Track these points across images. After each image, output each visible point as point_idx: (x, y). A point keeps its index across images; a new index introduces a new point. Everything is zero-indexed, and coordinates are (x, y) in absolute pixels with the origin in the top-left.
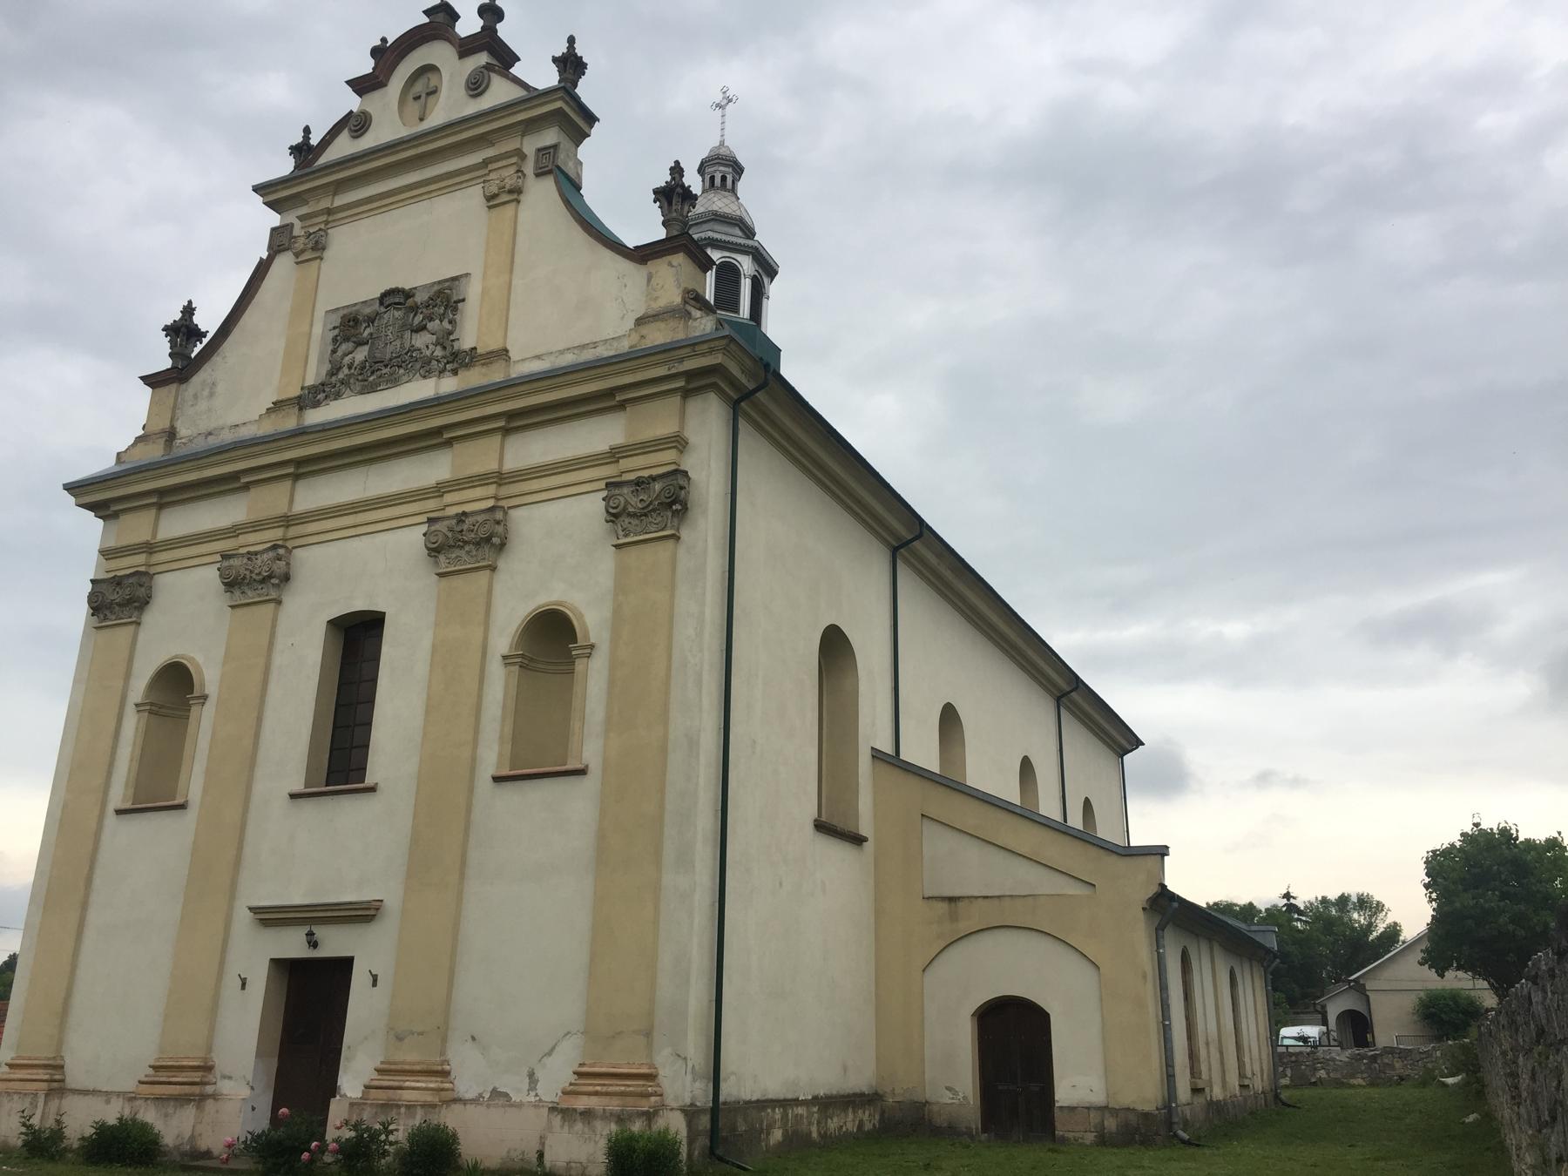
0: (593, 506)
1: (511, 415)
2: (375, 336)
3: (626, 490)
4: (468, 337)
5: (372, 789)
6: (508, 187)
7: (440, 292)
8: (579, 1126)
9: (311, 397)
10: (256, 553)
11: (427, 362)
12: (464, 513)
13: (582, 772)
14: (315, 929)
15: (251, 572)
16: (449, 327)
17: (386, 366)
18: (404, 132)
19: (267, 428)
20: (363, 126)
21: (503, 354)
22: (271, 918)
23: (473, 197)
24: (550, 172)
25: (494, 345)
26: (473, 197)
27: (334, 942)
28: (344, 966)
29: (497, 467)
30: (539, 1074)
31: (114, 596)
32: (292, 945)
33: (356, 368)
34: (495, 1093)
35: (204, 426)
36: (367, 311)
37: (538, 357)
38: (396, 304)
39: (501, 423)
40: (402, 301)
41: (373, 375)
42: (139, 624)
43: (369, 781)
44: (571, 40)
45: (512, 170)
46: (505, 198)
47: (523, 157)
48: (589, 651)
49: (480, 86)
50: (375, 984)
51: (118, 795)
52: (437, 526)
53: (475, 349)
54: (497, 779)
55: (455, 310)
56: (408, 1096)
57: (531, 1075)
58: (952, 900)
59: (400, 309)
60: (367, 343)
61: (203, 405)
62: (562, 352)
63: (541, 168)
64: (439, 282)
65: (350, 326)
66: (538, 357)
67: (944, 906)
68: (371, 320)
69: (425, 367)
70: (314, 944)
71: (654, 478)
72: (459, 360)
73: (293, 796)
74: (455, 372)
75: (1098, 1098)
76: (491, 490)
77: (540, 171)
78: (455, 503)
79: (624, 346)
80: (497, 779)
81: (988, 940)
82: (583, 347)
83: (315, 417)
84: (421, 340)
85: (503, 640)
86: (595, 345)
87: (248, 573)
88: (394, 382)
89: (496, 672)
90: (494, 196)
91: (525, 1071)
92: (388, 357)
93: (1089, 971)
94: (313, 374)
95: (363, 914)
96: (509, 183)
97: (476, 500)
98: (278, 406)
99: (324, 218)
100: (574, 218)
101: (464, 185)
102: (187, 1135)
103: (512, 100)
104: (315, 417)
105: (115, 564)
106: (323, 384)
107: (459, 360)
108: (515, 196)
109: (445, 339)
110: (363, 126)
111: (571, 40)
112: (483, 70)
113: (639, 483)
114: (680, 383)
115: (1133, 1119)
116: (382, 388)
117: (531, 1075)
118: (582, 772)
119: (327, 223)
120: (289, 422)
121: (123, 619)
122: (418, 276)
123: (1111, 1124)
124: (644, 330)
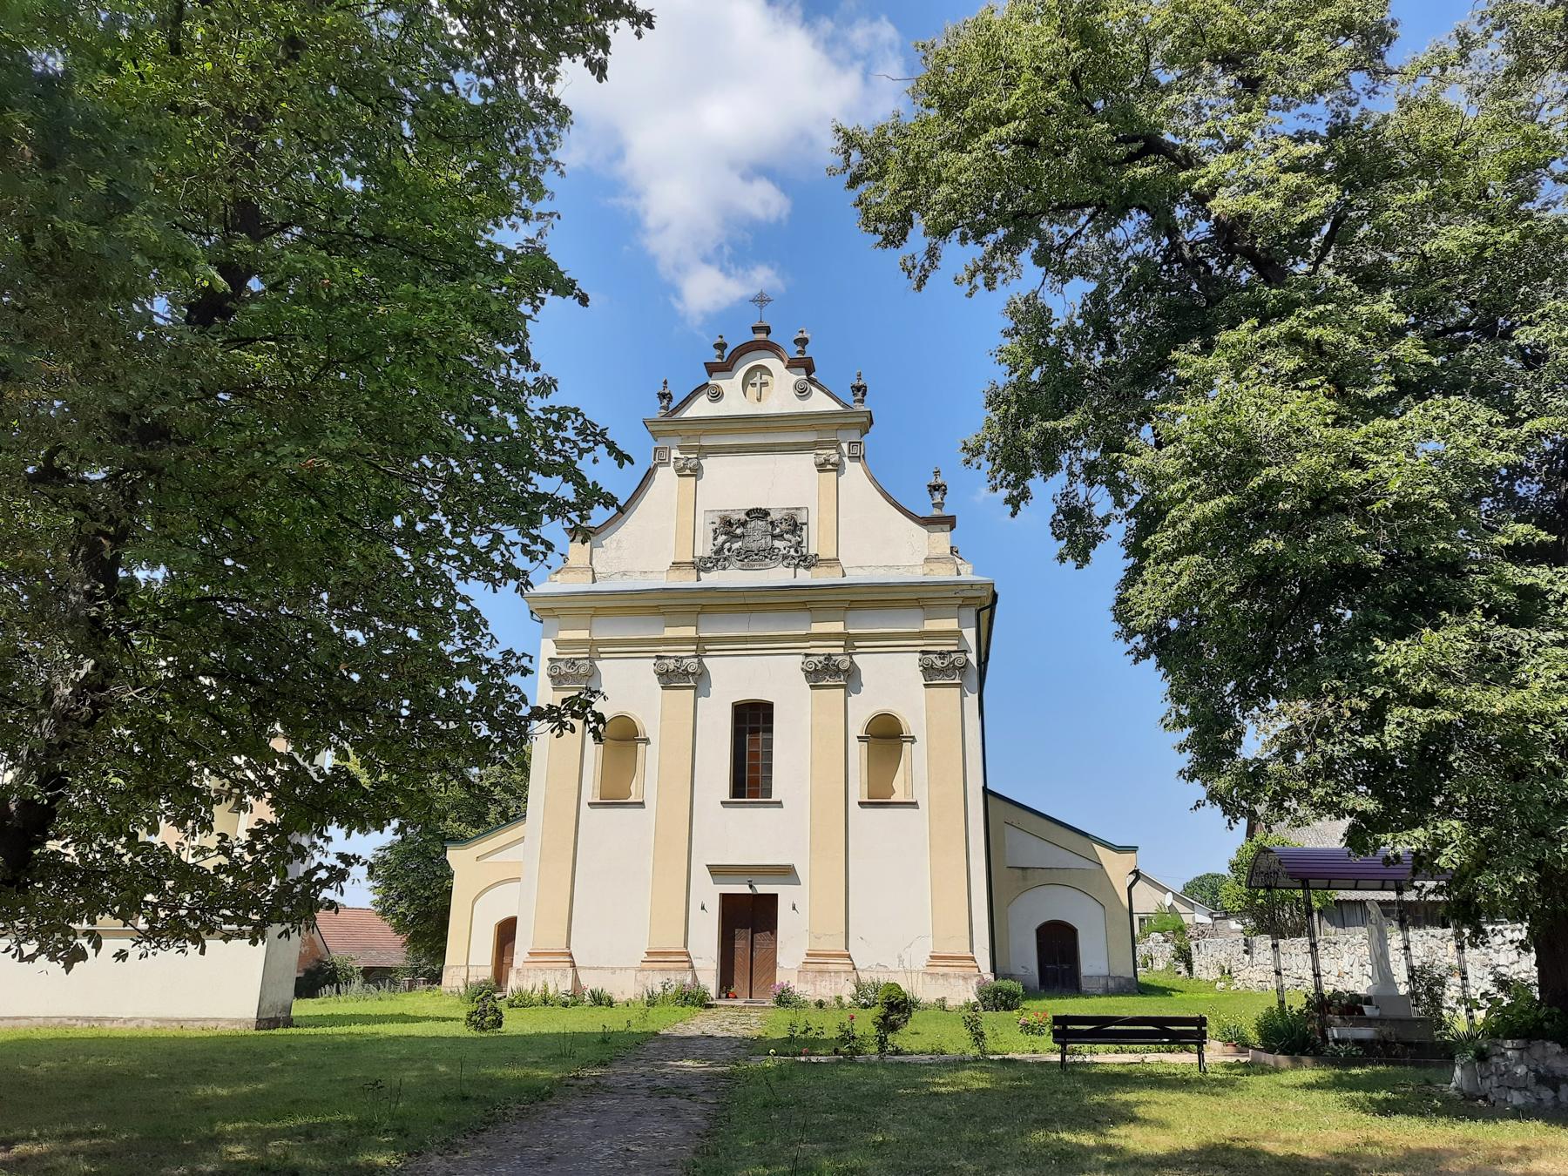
5: (779, 804)
8: (941, 981)
9: (701, 566)
13: (641, 805)
22: (717, 872)
26: (807, 461)
28: (773, 898)
36: (737, 517)
41: (749, 558)
43: (774, 798)
46: (829, 467)
51: (590, 793)
52: (810, 659)
54: (861, 804)
65: (728, 526)
67: (1020, 871)
68: (743, 524)
72: (808, 561)
75: (1105, 972)
85: (858, 728)
94: (705, 549)
95: (786, 873)
98: (677, 565)
107: (808, 561)
115: (1123, 981)
118: (914, 805)
120: (687, 580)
122: (777, 502)
123: (1111, 984)
124: (934, 566)
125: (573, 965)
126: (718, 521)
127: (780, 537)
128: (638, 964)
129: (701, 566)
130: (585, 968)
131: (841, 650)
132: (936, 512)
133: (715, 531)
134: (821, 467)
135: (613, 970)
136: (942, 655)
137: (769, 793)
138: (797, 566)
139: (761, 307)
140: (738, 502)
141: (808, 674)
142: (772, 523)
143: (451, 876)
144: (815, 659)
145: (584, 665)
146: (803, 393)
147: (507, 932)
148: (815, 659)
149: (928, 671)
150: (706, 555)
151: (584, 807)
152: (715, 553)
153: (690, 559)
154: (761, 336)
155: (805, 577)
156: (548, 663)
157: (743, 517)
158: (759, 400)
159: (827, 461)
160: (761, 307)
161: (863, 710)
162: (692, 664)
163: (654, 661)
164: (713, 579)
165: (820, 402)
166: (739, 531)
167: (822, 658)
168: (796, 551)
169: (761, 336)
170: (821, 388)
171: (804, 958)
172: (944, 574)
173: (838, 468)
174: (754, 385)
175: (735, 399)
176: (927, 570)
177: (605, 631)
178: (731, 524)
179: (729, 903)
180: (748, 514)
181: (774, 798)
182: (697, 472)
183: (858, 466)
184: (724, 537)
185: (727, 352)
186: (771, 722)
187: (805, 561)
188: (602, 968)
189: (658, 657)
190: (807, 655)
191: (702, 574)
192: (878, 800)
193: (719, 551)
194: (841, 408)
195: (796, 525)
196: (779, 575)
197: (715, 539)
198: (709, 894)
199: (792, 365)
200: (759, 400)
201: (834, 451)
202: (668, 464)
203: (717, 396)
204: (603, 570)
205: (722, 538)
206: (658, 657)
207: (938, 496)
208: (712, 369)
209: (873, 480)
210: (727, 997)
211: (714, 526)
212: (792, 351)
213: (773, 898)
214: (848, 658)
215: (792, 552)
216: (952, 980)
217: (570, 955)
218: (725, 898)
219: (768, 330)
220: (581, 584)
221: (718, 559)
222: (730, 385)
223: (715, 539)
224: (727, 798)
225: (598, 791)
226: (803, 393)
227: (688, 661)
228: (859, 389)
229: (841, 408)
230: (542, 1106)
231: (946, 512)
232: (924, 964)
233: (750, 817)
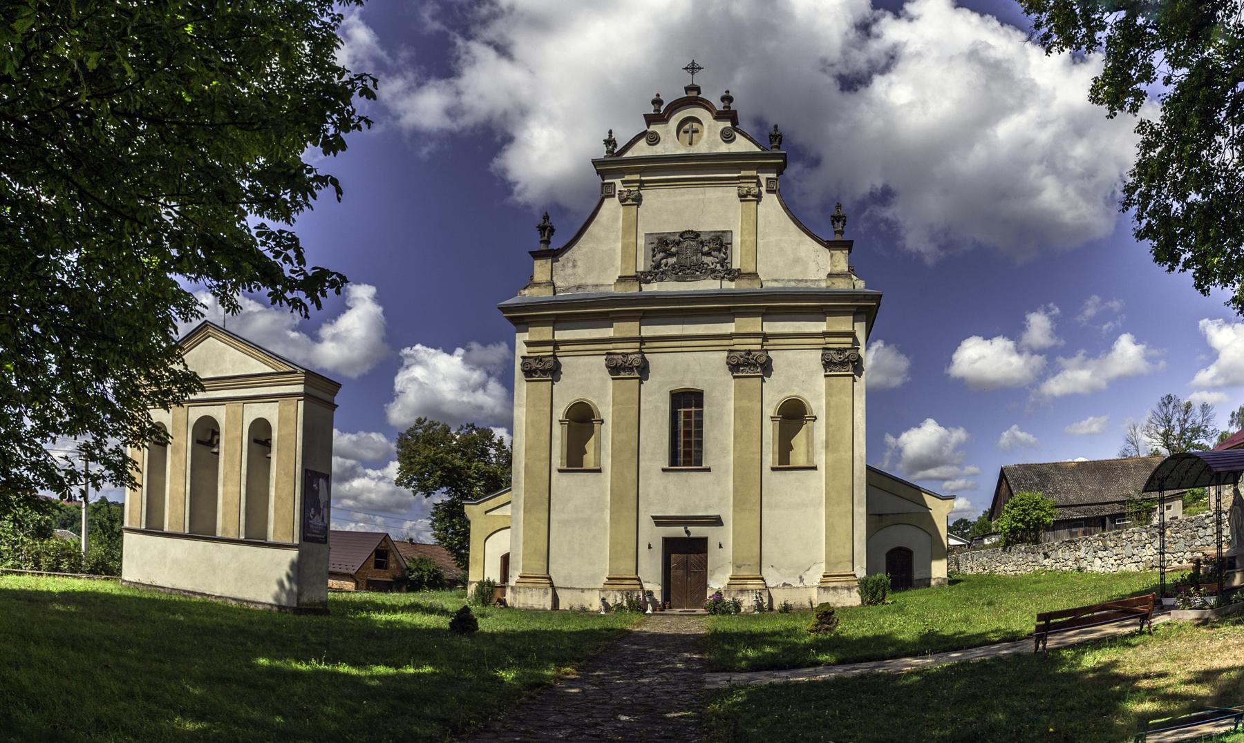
5: (708, 470)
7: (718, 238)
8: (831, 592)
9: (641, 278)
10: (628, 354)
11: (713, 271)
12: (749, 350)
19: (622, 290)
21: (754, 275)
22: (660, 521)
25: (751, 269)
27: (696, 531)
30: (804, 577)
31: (535, 365)
32: (678, 531)
34: (785, 584)
35: (572, 282)
36: (672, 238)
41: (684, 271)
44: (611, 132)
53: (739, 269)
54: (560, 471)
55: (726, 248)
56: (749, 587)
57: (801, 577)
58: (880, 515)
60: (675, 255)
61: (569, 271)
62: (789, 281)
64: (715, 232)
65: (662, 244)
68: (678, 243)
69: (713, 273)
72: (734, 275)
74: (732, 280)
76: (760, 340)
78: (743, 345)
80: (773, 469)
81: (893, 527)
83: (654, 287)
84: (707, 260)
85: (770, 410)
88: (697, 279)
89: (768, 424)
90: (745, 196)
91: (798, 576)
93: (929, 538)
95: (717, 521)
97: (754, 345)
102: (783, 603)
105: (532, 349)
106: (650, 272)
107: (734, 275)
109: (723, 262)
111: (611, 132)
114: (855, 310)
115: (940, 581)
117: (801, 577)
120: (632, 289)
122: (707, 224)
124: (835, 280)
125: (552, 585)
126: (656, 241)
127: (708, 254)
128: (601, 586)
130: (561, 588)
131: (759, 347)
132: (838, 237)
133: (653, 250)
134: (743, 197)
135: (583, 590)
136: (840, 351)
137: (699, 462)
138: (722, 278)
139: (693, 73)
140: (672, 226)
141: (740, 196)
142: (702, 243)
143: (469, 522)
144: (737, 354)
145: (549, 361)
146: (727, 137)
147: (506, 559)
148: (737, 354)
149: (828, 364)
150: (647, 270)
151: (555, 474)
152: (655, 268)
153: (634, 274)
154: (694, 94)
155: (729, 285)
156: (521, 360)
157: (677, 238)
158: (691, 144)
159: (748, 193)
160: (693, 73)
161: (774, 393)
162: (635, 359)
163: (605, 357)
164: (654, 287)
165: (742, 145)
166: (673, 250)
167: (743, 353)
168: (722, 266)
169: (694, 94)
170: (744, 134)
171: (728, 581)
172: (842, 285)
173: (758, 198)
174: (686, 132)
175: (670, 144)
176: (829, 283)
178: (667, 244)
179: (670, 545)
181: (704, 466)
182: (638, 200)
183: (774, 197)
184: (662, 255)
185: (663, 108)
187: (729, 274)
188: (574, 588)
190: (731, 351)
191: (643, 285)
192: (784, 463)
193: (658, 266)
194: (758, 150)
195: (721, 245)
196: (709, 285)
197: (654, 256)
198: (653, 536)
199: (719, 116)
200: (691, 144)
201: (754, 185)
202: (614, 196)
203: (654, 140)
204: (562, 284)
205: (659, 256)
206: (608, 354)
207: (839, 226)
208: (650, 120)
209: (787, 208)
210: (670, 608)
211: (653, 246)
212: (719, 106)
213: (703, 541)
214: (765, 353)
215: (719, 267)
216: (840, 591)
217: (550, 579)
219: (698, 89)
220: (544, 294)
221: (655, 273)
222: (667, 131)
223: (654, 256)
224: (667, 466)
225: (565, 461)
226: (727, 137)
227: (633, 356)
228: (776, 137)
229: (758, 150)
231: (846, 238)
232: (819, 581)
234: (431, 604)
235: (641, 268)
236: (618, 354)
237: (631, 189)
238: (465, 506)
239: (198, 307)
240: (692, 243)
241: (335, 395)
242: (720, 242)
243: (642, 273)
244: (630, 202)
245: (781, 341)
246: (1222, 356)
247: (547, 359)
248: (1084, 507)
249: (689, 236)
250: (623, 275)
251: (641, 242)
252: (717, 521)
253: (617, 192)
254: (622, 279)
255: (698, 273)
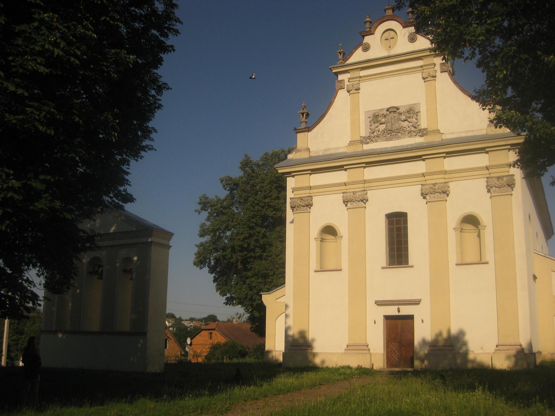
0: (482, 183)
1: (447, 153)
2: (387, 122)
3: (494, 179)
4: (423, 124)
5: (412, 267)
6: (431, 75)
9: (365, 140)
13: (487, 263)
14: (400, 307)
15: (355, 198)
16: (416, 121)
17: (393, 132)
18: (385, 54)
20: (367, 49)
22: (379, 303)
23: (418, 76)
24: (446, 71)
26: (418, 76)
27: (405, 311)
28: (411, 318)
29: (489, 164)
32: (392, 311)
33: (381, 132)
36: (381, 113)
37: (452, 133)
38: (394, 111)
39: (310, 172)
40: (396, 110)
41: (391, 133)
42: (310, 212)
45: (432, 70)
47: (435, 65)
48: (485, 228)
49: (414, 39)
50: (375, 323)
54: (315, 271)
55: (417, 116)
59: (396, 113)
62: (461, 132)
63: (443, 70)
65: (375, 118)
66: (452, 133)
70: (399, 311)
71: (504, 176)
72: (423, 133)
73: (383, 268)
77: (443, 71)
78: (431, 180)
79: (484, 132)
80: (315, 271)
82: (469, 131)
86: (473, 131)
87: (354, 198)
88: (399, 138)
92: (394, 129)
94: (363, 132)
95: (417, 302)
96: (432, 74)
99: (359, 79)
100: (458, 88)
101: (413, 73)
103: (351, 63)
104: (366, 147)
107: (423, 133)
108: (434, 79)
110: (367, 49)
112: (414, 34)
113: (498, 178)
116: (394, 139)
119: (359, 81)
121: (304, 210)
122: (402, 102)
129: (365, 140)
133: (370, 122)
137: (407, 262)
140: (383, 104)
149: (346, 202)
150: (367, 136)
151: (312, 274)
153: (359, 139)
157: (385, 112)
166: (383, 120)
177: (452, 163)
180: (387, 110)
186: (407, 223)
189: (343, 193)
213: (411, 318)
218: (387, 318)
230: (228, 411)
233: (400, 272)
234: (223, 394)
235: (363, 134)
236: (351, 192)
237: (355, 83)
238: (262, 295)
239: (508, 166)
240: (395, 115)
241: (170, 240)
242: (412, 112)
243: (364, 138)
244: (353, 91)
245: (458, 175)
246: (513, 168)
247: (306, 199)
248: (432, 200)
249: (392, 110)
250: (353, 140)
251: (362, 117)
252: (417, 302)
253: (346, 86)
254: (352, 143)
255: (400, 134)
